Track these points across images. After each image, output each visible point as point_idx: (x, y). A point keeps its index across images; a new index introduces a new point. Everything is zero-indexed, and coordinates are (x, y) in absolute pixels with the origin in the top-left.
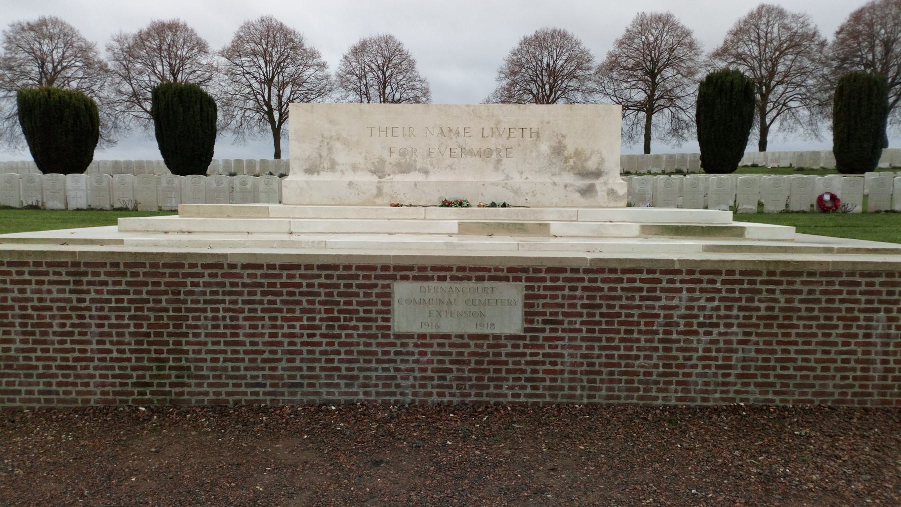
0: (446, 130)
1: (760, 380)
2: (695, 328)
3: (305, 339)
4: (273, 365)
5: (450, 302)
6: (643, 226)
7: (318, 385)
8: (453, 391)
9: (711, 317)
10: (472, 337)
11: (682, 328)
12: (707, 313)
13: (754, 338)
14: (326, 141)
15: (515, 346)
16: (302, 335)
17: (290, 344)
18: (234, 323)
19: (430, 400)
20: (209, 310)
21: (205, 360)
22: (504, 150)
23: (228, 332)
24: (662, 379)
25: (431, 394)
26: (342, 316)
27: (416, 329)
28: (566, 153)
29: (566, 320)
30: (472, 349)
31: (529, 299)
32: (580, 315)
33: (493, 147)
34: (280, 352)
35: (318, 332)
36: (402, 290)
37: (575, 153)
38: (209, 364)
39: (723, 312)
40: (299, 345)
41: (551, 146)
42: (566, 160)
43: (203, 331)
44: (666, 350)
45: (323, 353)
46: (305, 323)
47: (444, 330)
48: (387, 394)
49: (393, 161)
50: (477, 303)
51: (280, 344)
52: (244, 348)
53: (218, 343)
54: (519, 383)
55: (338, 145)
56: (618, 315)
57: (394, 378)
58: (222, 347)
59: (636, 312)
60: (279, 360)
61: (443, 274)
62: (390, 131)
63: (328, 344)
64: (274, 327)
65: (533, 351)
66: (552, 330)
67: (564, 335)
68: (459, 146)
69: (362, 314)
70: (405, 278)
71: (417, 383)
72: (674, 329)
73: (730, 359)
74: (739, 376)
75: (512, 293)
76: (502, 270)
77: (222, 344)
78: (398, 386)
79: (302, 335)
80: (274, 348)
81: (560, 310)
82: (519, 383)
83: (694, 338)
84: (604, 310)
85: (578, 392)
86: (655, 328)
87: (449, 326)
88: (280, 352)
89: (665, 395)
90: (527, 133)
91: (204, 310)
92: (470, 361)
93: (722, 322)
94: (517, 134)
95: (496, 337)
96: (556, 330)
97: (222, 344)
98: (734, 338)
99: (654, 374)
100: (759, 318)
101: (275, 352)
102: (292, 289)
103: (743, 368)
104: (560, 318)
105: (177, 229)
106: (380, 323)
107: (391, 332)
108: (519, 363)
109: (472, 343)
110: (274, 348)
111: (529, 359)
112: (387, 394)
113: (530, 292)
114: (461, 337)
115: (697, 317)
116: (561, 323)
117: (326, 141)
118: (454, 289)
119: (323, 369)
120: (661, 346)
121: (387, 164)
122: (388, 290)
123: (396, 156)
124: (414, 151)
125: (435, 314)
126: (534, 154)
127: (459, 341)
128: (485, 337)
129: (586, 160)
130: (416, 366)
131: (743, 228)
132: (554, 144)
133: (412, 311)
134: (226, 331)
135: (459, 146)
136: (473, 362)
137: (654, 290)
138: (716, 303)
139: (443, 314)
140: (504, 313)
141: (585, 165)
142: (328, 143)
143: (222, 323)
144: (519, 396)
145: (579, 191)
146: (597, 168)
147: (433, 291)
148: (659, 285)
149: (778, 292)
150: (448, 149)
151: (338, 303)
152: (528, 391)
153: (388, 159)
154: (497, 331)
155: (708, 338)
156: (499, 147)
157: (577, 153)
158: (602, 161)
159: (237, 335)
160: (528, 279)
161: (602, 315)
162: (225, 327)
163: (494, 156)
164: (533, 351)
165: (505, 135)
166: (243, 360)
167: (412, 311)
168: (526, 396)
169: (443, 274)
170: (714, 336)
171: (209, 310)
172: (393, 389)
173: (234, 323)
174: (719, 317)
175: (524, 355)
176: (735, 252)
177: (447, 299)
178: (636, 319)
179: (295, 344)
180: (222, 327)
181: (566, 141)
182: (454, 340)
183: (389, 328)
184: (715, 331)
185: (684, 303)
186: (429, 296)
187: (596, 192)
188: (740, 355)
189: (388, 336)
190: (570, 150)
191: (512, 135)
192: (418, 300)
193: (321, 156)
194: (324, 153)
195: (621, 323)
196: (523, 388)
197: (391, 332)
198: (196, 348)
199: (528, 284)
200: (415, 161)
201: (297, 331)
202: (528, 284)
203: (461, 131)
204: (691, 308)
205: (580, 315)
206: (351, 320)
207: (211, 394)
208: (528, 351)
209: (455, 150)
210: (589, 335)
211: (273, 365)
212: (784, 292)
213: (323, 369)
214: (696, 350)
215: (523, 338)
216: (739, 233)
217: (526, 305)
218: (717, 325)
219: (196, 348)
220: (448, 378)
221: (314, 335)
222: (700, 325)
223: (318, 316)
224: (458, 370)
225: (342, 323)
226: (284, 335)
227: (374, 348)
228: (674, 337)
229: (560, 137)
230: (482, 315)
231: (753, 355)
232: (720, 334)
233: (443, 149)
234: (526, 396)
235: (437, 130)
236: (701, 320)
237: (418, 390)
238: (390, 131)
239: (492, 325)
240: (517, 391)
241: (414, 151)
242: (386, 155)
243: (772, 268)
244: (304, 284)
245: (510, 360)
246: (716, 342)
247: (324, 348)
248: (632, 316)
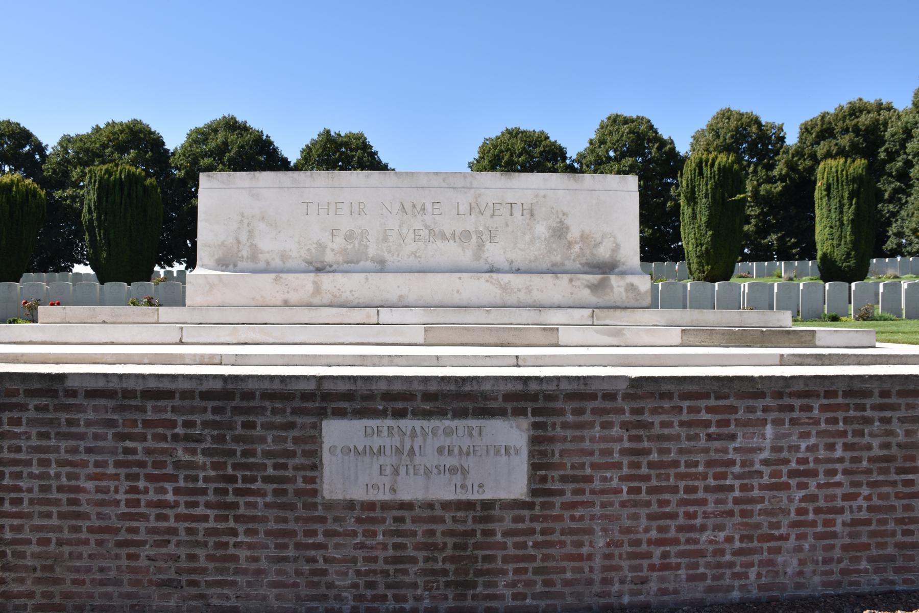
0: (408, 207)
1: (874, 552)
2: (784, 479)
3: (182, 510)
4: (132, 550)
5: (412, 451)
6: (683, 331)
7: (203, 584)
8: (419, 592)
9: (805, 461)
10: (446, 505)
11: (766, 479)
12: (800, 455)
13: (865, 491)
14: (246, 222)
15: (518, 519)
16: (176, 504)
17: (159, 517)
18: (73, 483)
19: (382, 607)
20: (35, 462)
21: (28, 542)
22: (487, 232)
23: (63, 497)
24: (738, 559)
25: (384, 598)
26: (239, 474)
27: (358, 494)
28: (569, 236)
29: (597, 475)
30: (450, 525)
31: (539, 442)
32: (618, 466)
33: (472, 229)
34: (142, 530)
35: (202, 499)
36: (336, 433)
37: (582, 236)
38: (36, 549)
39: (822, 454)
40: (172, 519)
41: (550, 228)
42: (570, 245)
43: (26, 496)
44: (743, 514)
45: (210, 532)
46: (182, 484)
47: (405, 495)
48: (314, 598)
49: (335, 246)
50: (456, 450)
51: (144, 517)
52: (88, 523)
53: (49, 515)
54: (524, 577)
55: (262, 226)
56: (675, 464)
57: (324, 573)
58: (55, 521)
59: (701, 458)
60: (142, 543)
61: (400, 405)
62: (332, 208)
63: (218, 518)
64: (133, 490)
65: (545, 525)
66: (576, 492)
67: (594, 498)
68: (426, 226)
69: (270, 471)
70: (340, 414)
71: (361, 581)
72: (755, 482)
73: (832, 523)
74: (845, 548)
75: (513, 434)
76: (495, 399)
77: (55, 516)
78: (330, 585)
79: (176, 504)
80: (134, 524)
81: (587, 460)
82: (524, 577)
83: (783, 495)
84: (654, 457)
85: (616, 587)
86: (728, 482)
87: (412, 490)
88: (142, 530)
89: (742, 582)
90: (517, 212)
91: (28, 463)
92: (445, 544)
93: (821, 468)
94: (505, 211)
95: (487, 505)
96: (581, 492)
97: (55, 516)
98: (839, 491)
99: (728, 551)
100: (870, 460)
101: (135, 531)
102: (160, 430)
103: (851, 535)
104: (588, 471)
105: (28, 340)
106: (300, 484)
107: (319, 500)
108: (524, 546)
109: (448, 516)
110: (134, 524)
111: (539, 538)
112: (314, 598)
113: (540, 432)
114: (430, 505)
115: (787, 462)
116: (589, 479)
117: (246, 222)
118: (418, 430)
119: (210, 558)
120: (736, 509)
121: (328, 251)
122: (312, 432)
123: (339, 241)
124: (364, 234)
125: (388, 470)
126: (527, 238)
127: (427, 513)
128: (469, 505)
129: (597, 245)
130: (359, 554)
131: (814, 332)
132: (555, 225)
133: (352, 464)
134: (60, 496)
135: (426, 226)
136: (450, 545)
137: (727, 423)
138: (813, 440)
139: (403, 470)
140: (499, 465)
141: (595, 252)
142: (249, 225)
143: (54, 484)
144: (524, 597)
145: (588, 287)
146: (611, 256)
147: (385, 433)
148: (733, 417)
149: (895, 421)
150: (411, 231)
151: (232, 453)
152: (539, 588)
153: (330, 245)
154: (488, 496)
155: (803, 493)
156: (481, 228)
157: (584, 238)
158: (617, 248)
159: (76, 502)
160: (535, 412)
161: (651, 465)
162: (60, 489)
163: (474, 239)
164: (545, 525)
165: (488, 212)
166: (86, 542)
167: (352, 464)
168: (535, 596)
169: (400, 405)
170: (812, 489)
171: (35, 462)
172: (323, 590)
173: (73, 483)
174: (817, 460)
175: (532, 532)
176: (22, 355)
177: (407, 447)
178: (701, 469)
179: (165, 518)
180: (54, 488)
181: (568, 222)
182: (417, 512)
183: (315, 492)
184: (813, 483)
185: (768, 443)
186: (376, 442)
187: (612, 288)
188: (847, 516)
189: (314, 506)
190: (574, 233)
191: (497, 213)
192: (360, 449)
193: (239, 242)
194: (244, 238)
195: (680, 476)
196: (530, 584)
197: (319, 500)
198: (16, 522)
199: (537, 419)
200: (366, 247)
201: (170, 497)
202: (537, 419)
203: (429, 207)
204: (779, 449)
205: (618, 466)
206: (253, 480)
207: (38, 596)
208: (538, 527)
209: (421, 233)
210: (632, 497)
211: (132, 550)
212: (902, 420)
213: (210, 558)
214: (786, 512)
215: (530, 506)
216: (808, 339)
217: (531, 454)
218: (814, 474)
219: (16, 522)
220: (411, 571)
221: (195, 505)
222: (793, 474)
223: (202, 475)
224: (427, 559)
225: (240, 485)
226: (150, 504)
227: (291, 526)
228: (756, 493)
229: (561, 216)
230: (465, 472)
231: (864, 515)
232: (819, 486)
233: (405, 231)
234: (535, 596)
235: (397, 206)
236: (793, 465)
237: (362, 591)
238: (332, 208)
239: (481, 486)
240: (520, 588)
241: (364, 234)
242: (326, 238)
243: (886, 386)
244: (180, 423)
245: (510, 541)
246: (813, 498)
247: (211, 524)
248: (696, 464)
